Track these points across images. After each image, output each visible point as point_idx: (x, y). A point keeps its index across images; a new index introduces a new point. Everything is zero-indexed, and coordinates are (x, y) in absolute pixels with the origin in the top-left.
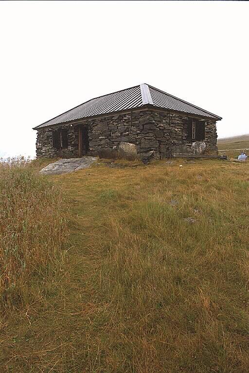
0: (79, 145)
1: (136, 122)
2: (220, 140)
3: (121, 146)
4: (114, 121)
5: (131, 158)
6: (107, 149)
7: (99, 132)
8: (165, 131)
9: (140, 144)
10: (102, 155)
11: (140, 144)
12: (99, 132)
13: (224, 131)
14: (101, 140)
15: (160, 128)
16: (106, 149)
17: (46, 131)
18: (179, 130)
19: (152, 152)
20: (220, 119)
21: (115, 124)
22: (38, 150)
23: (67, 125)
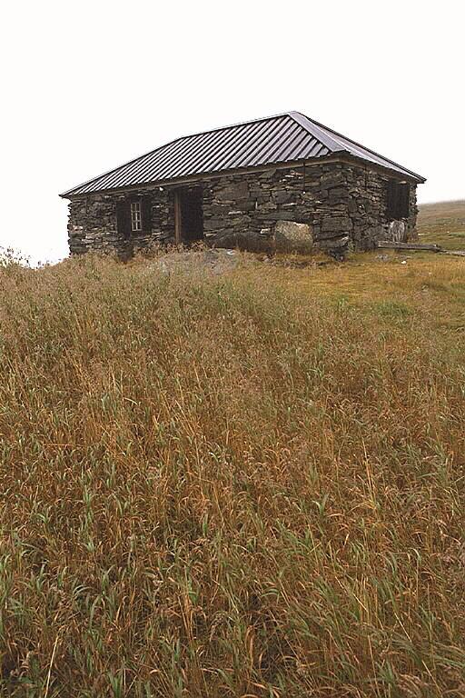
0: (177, 227)
1: (314, 184)
2: (425, 207)
3: (279, 229)
4: (265, 181)
5: (303, 249)
6: (247, 233)
7: (227, 202)
8: (359, 201)
9: (320, 224)
10: (244, 245)
11: (320, 224)
12: (227, 202)
13: (424, 196)
14: (232, 217)
15: (354, 195)
16: (244, 234)
17: (95, 201)
18: (377, 199)
19: (347, 238)
20: (423, 181)
21: (265, 186)
22: (76, 245)
23: (151, 188)
